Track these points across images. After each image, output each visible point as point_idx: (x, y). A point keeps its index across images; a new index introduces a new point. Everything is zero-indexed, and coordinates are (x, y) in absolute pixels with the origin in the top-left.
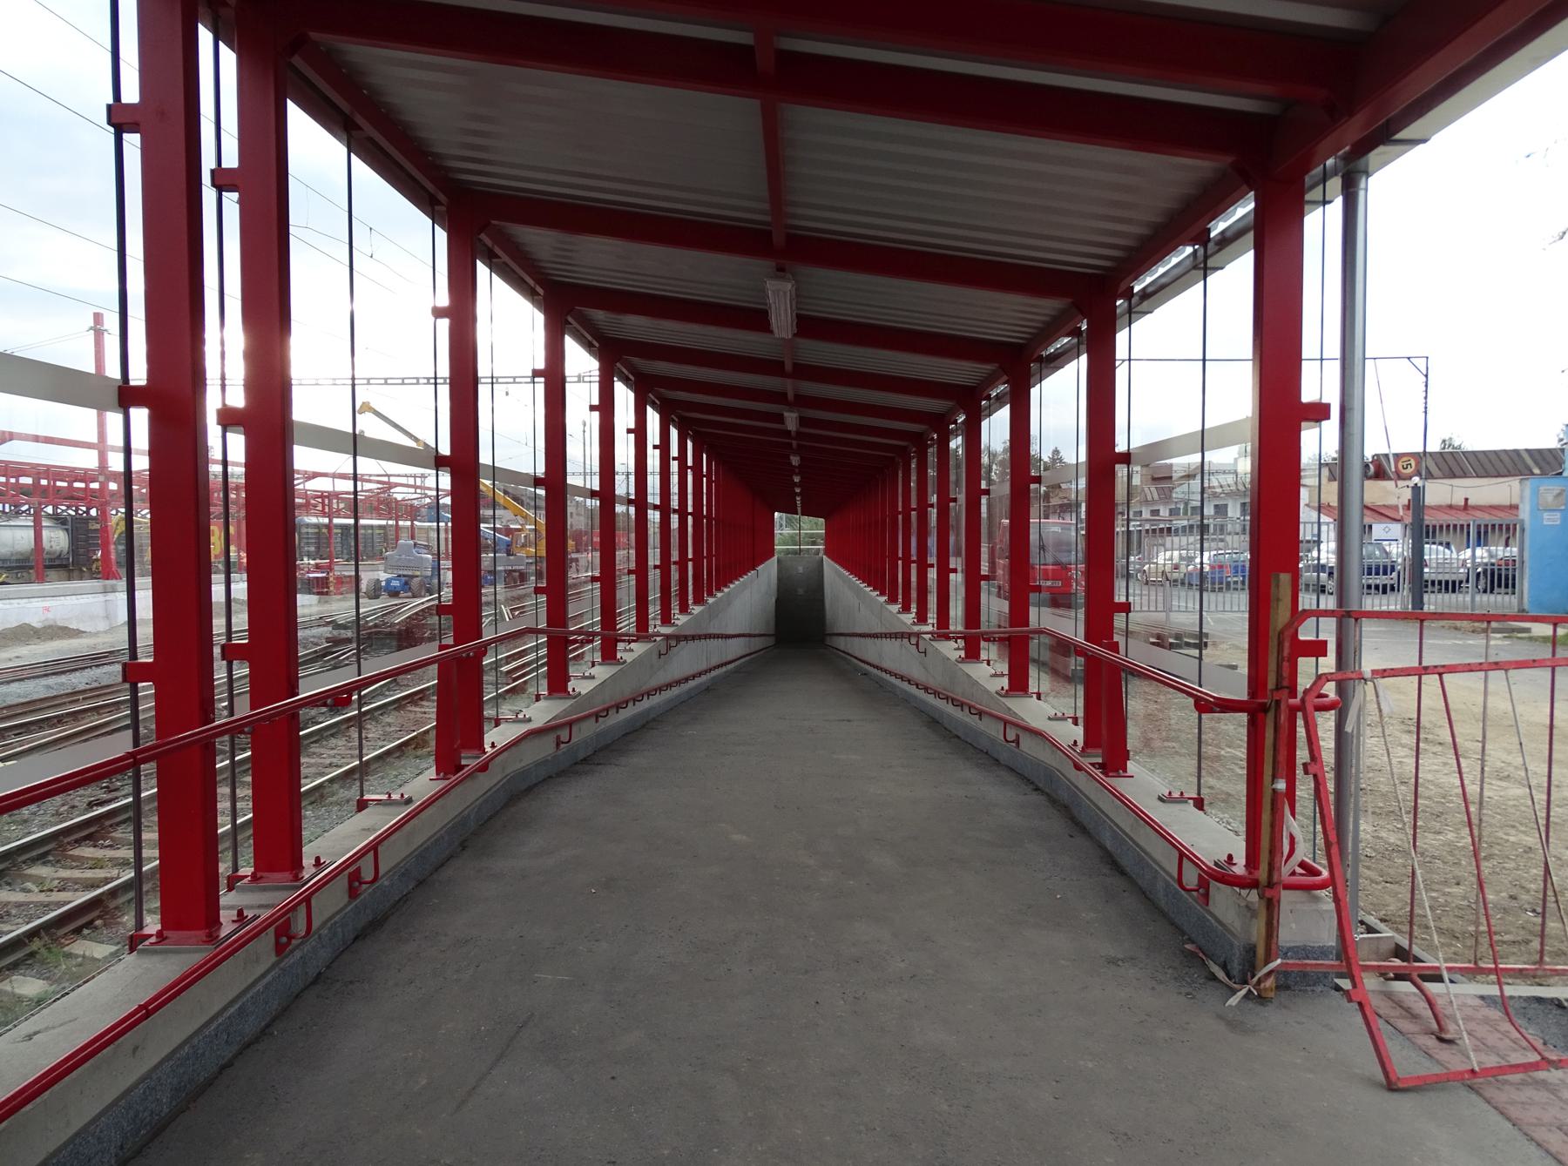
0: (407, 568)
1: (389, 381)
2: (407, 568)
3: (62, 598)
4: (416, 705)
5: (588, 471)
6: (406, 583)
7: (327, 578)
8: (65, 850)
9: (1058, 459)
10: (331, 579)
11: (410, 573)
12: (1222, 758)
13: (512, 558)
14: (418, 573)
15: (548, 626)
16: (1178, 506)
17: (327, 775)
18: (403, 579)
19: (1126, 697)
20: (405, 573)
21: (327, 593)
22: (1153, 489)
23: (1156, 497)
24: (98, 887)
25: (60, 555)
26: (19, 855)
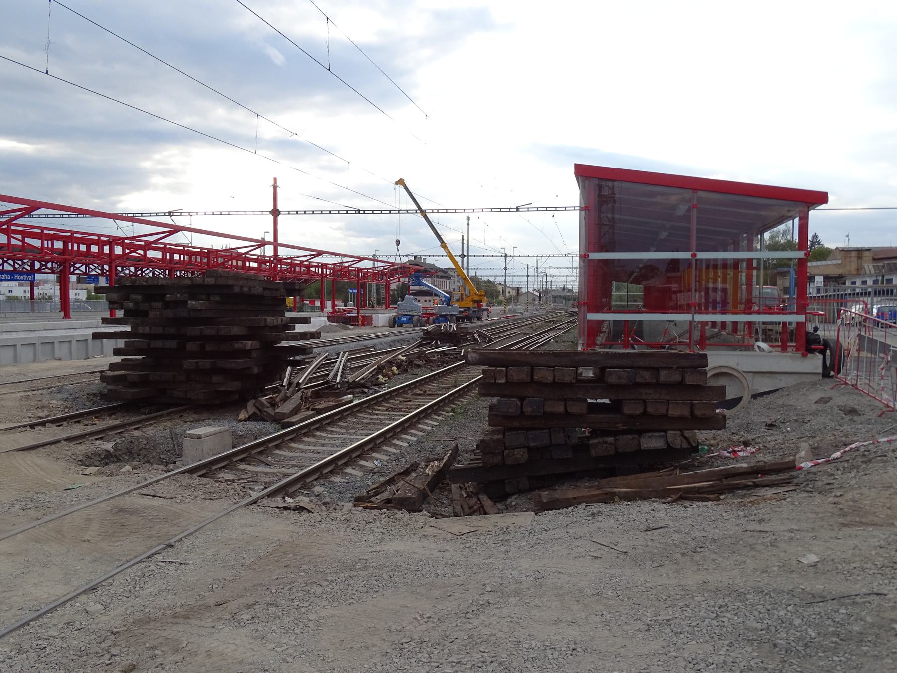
0: (410, 311)
1: (320, 212)
2: (410, 311)
3: (73, 330)
4: (356, 417)
5: (465, 253)
6: (410, 319)
7: (358, 316)
8: (313, 433)
9: (816, 242)
10: (360, 317)
11: (411, 313)
12: (452, 273)
13: (450, 307)
14: (415, 314)
15: (588, 320)
16: (878, 278)
17: (388, 425)
18: (408, 317)
19: (843, 363)
20: (409, 313)
21: (358, 325)
22: (871, 266)
23: (873, 271)
24: (319, 461)
25: (472, 313)
26: (253, 450)
